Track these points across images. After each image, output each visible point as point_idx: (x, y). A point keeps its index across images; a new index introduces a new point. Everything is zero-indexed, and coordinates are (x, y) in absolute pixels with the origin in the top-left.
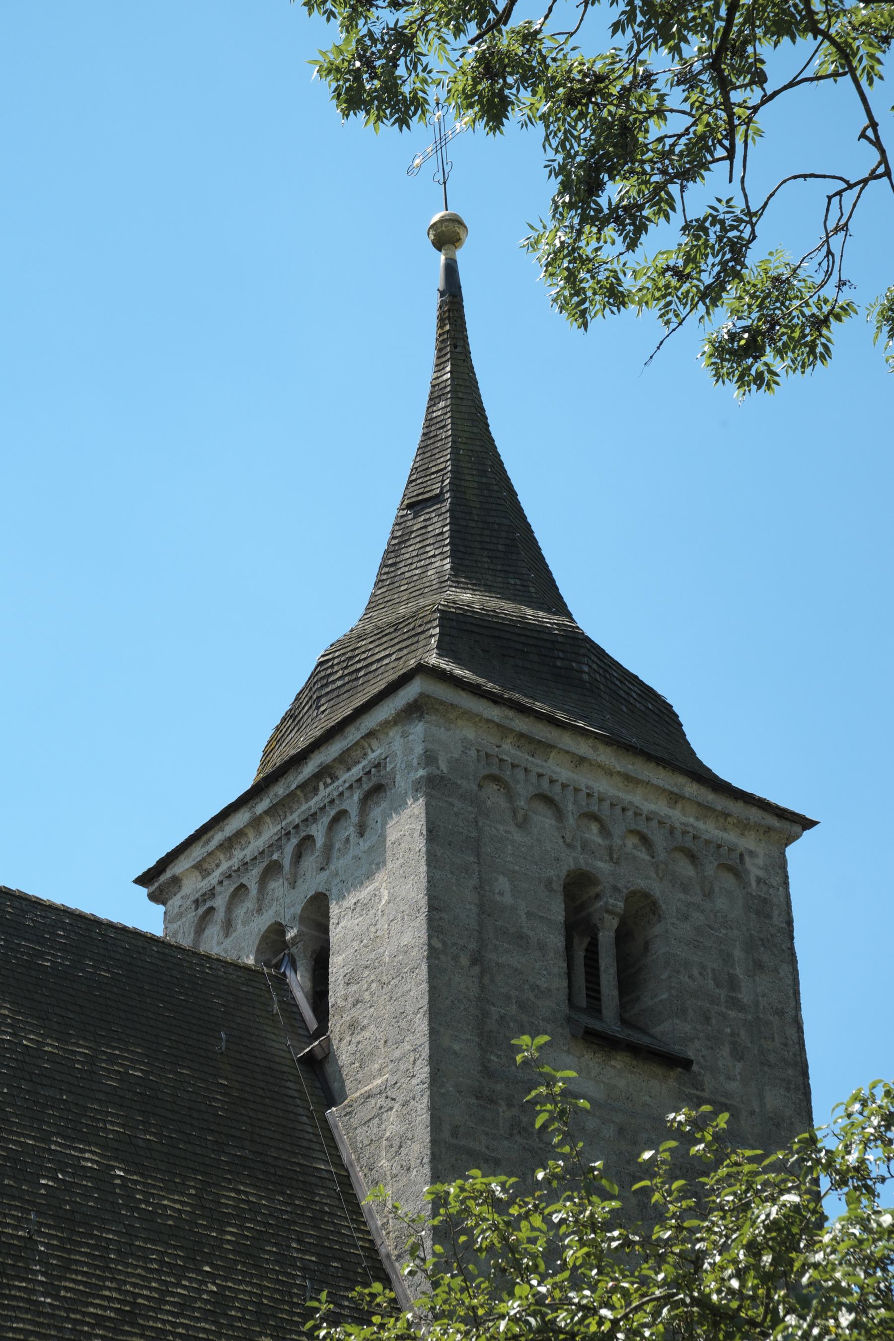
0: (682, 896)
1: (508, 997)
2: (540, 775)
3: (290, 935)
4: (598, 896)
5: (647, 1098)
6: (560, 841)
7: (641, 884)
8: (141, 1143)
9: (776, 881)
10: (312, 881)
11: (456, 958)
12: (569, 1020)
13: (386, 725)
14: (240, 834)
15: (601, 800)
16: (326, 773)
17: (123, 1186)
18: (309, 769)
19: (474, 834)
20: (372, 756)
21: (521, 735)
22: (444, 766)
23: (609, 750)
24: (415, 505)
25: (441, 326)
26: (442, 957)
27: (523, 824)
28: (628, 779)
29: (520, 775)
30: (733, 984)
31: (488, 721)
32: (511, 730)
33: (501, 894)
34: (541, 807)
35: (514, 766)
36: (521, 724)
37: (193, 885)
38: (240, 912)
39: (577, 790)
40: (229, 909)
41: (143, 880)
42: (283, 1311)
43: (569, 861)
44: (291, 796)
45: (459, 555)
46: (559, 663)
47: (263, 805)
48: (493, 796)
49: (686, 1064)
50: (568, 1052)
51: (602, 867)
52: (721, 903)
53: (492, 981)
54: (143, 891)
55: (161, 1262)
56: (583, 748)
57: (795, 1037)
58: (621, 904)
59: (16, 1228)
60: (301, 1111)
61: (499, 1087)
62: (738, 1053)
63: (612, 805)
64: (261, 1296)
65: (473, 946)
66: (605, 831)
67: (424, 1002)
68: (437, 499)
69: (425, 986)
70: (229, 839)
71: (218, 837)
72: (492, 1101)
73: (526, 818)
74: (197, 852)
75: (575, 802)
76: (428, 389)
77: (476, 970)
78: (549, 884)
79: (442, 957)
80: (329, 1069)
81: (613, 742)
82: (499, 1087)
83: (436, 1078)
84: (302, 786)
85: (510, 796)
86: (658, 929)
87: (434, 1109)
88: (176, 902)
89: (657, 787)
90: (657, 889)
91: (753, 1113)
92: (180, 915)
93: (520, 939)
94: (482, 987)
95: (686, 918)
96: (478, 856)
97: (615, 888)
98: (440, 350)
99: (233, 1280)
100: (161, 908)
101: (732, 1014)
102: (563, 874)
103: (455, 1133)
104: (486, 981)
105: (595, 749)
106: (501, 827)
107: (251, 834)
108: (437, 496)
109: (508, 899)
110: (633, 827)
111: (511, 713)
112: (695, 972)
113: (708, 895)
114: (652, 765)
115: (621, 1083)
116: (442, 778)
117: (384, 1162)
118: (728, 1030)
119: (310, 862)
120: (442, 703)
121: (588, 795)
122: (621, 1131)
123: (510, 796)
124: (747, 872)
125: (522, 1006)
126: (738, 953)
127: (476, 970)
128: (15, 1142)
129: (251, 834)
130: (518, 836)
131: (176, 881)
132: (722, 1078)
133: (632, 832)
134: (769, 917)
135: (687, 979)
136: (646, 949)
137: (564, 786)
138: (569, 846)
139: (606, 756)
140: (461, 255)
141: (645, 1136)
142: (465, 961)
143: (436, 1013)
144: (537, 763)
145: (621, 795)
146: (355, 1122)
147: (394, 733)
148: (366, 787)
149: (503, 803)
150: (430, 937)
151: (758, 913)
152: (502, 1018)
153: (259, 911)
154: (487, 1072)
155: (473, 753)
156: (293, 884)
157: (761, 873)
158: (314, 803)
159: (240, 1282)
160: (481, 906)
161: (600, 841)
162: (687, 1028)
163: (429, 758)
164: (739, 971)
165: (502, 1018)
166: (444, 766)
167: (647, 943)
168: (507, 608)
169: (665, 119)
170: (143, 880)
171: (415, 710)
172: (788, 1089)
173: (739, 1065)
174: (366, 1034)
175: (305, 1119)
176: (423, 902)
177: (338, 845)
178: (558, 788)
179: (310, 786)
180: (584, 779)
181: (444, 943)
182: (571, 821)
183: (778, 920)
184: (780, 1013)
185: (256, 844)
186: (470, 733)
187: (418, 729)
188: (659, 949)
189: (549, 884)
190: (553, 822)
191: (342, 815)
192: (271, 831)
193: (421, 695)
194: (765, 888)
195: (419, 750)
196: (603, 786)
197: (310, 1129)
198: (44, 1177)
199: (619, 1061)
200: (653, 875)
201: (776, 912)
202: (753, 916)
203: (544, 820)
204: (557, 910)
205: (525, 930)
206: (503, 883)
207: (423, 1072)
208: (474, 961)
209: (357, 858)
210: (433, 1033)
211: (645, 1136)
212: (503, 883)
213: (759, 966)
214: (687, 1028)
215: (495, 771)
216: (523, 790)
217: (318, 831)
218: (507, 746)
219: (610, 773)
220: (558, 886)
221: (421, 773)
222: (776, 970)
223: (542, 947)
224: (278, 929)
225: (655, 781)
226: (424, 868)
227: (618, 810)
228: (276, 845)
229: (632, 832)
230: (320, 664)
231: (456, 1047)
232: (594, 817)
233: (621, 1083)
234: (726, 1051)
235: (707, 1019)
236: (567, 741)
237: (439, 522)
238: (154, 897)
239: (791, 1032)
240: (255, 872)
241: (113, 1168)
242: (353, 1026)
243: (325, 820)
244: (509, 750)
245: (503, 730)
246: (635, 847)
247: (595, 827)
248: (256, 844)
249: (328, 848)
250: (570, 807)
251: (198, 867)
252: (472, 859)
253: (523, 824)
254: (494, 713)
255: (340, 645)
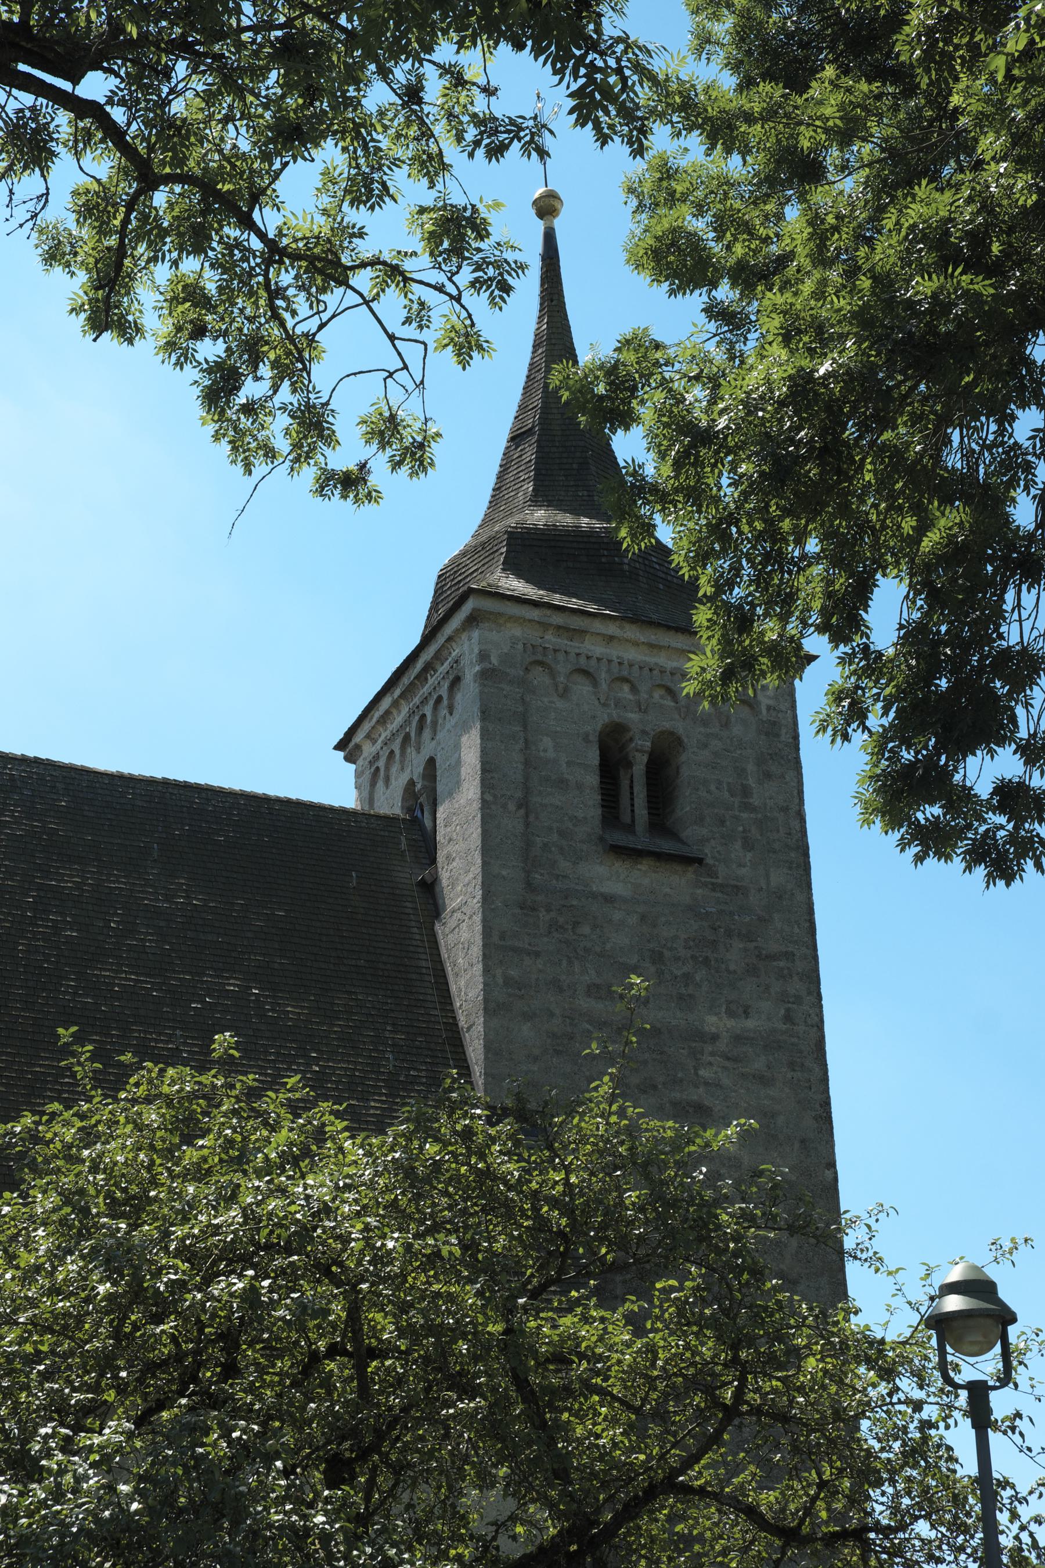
0: (702, 729)
1: (550, 829)
2: (578, 655)
3: (419, 786)
4: (631, 740)
5: (668, 890)
6: (596, 702)
7: (667, 725)
8: (276, 966)
9: (784, 706)
10: (428, 749)
11: (504, 806)
12: (601, 839)
13: (458, 631)
14: (388, 713)
15: (631, 666)
16: (428, 667)
17: (257, 1000)
18: (419, 665)
19: (521, 709)
20: (454, 654)
21: (559, 627)
22: (495, 661)
23: (634, 627)
24: (516, 439)
25: (542, 285)
26: (493, 807)
27: (565, 693)
28: (651, 646)
29: (561, 656)
30: (746, 791)
31: (530, 621)
32: (550, 625)
33: (545, 751)
34: (579, 678)
35: (555, 651)
36: (558, 619)
37: (369, 750)
38: (394, 769)
39: (610, 661)
40: (387, 768)
41: (339, 747)
42: (370, 1079)
43: (604, 717)
44: (412, 684)
45: (540, 479)
46: (603, 560)
47: (397, 692)
48: (539, 677)
49: (700, 861)
50: (601, 863)
51: (633, 717)
52: (737, 730)
53: (537, 818)
54: (341, 754)
55: (278, 1054)
56: (612, 629)
57: (798, 828)
58: (649, 744)
59: (167, 1042)
60: (413, 924)
61: (539, 898)
62: (748, 845)
63: (641, 668)
64: (355, 1069)
65: (519, 794)
66: (634, 689)
67: (479, 842)
68: (530, 432)
69: (479, 830)
70: (382, 716)
71: (377, 714)
72: (533, 909)
73: (566, 690)
74: (366, 726)
75: (609, 671)
76: (532, 337)
77: (522, 811)
78: (586, 738)
79: (493, 807)
80: (437, 889)
81: (635, 618)
82: (539, 898)
83: (486, 899)
84: (417, 677)
85: (553, 674)
86: (683, 758)
87: (485, 921)
88: (360, 762)
89: (676, 649)
90: (680, 727)
91: (760, 890)
92: (363, 772)
93: (562, 784)
94: (527, 825)
95: (705, 746)
96: (525, 727)
97: (644, 732)
98: (541, 304)
99: (334, 1061)
100: (353, 766)
101: (745, 815)
102: (599, 727)
103: (502, 937)
104: (531, 818)
105: (621, 628)
106: (546, 700)
107: (395, 712)
108: (530, 429)
109: (551, 754)
110: (659, 682)
111: (548, 612)
112: (713, 787)
113: (726, 725)
114: (672, 633)
115: (646, 882)
116: (493, 670)
117: (460, 960)
118: (741, 829)
119: (427, 733)
120: (491, 613)
121: (620, 663)
122: (643, 918)
123: (553, 674)
124: (759, 703)
125: (562, 833)
126: (751, 767)
127: (522, 811)
128: (175, 979)
129: (395, 712)
130: (560, 704)
131: (358, 747)
132: (734, 866)
133: (659, 686)
134: (778, 735)
135: (705, 794)
136: (678, 772)
137: (599, 660)
138: (604, 705)
139: (632, 632)
140: (558, 223)
141: (663, 919)
142: (512, 807)
143: (486, 849)
144: (574, 646)
145: (647, 659)
146: (447, 930)
147: (464, 636)
148: (451, 677)
149: (547, 680)
150: (483, 793)
151: (767, 734)
152: (545, 845)
153: (402, 769)
154: (530, 886)
155: (520, 646)
156: (418, 750)
157: (771, 702)
158: (425, 690)
159: (339, 1062)
160: (527, 763)
161: (631, 697)
162: (704, 831)
163: (483, 656)
164: (751, 782)
165: (545, 845)
166: (495, 661)
167: (678, 768)
168: (566, 520)
169: (583, 125)
170: (339, 747)
171: (472, 620)
172: (790, 868)
173: (749, 855)
174: (454, 864)
175: (415, 930)
176: (479, 767)
177: (440, 721)
178: (593, 662)
179: (422, 677)
180: (614, 652)
181: (495, 796)
182: (604, 686)
183: (785, 737)
184: (785, 810)
185: (399, 719)
186: (517, 632)
187: (476, 634)
188: (685, 772)
189: (586, 738)
190: (591, 689)
191: (439, 699)
192: (405, 710)
193: (474, 610)
194: (774, 714)
195: (476, 651)
196: (631, 654)
197: (418, 937)
198: (195, 1002)
199: (645, 865)
200: (677, 717)
201: (784, 731)
202: (763, 737)
203: (582, 689)
204: (593, 756)
205: (566, 776)
206: (547, 742)
207: (479, 894)
208: (519, 806)
209: (449, 731)
210: (485, 864)
211: (663, 919)
212: (547, 742)
213: (768, 776)
214: (704, 831)
215: (540, 658)
216: (562, 668)
217: (428, 710)
218: (549, 636)
219: (636, 644)
220: (594, 738)
221: (477, 668)
222: (782, 776)
223: (579, 786)
224: (411, 783)
225: (674, 644)
226: (479, 741)
227: (646, 671)
228: (407, 722)
229: (659, 686)
230: (439, 577)
231: (504, 873)
232: (625, 680)
233: (646, 882)
234: (738, 845)
235: (722, 822)
236: (597, 626)
237: (529, 452)
238: (349, 759)
239: (795, 824)
240: (399, 741)
241: (251, 988)
242: (449, 858)
243: (431, 703)
244: (551, 639)
245: (544, 626)
246: (662, 697)
247: (626, 688)
248: (399, 719)
249: (435, 723)
250: (603, 675)
251: (368, 736)
252: (518, 728)
253: (565, 693)
254: (535, 614)
255: (453, 561)
